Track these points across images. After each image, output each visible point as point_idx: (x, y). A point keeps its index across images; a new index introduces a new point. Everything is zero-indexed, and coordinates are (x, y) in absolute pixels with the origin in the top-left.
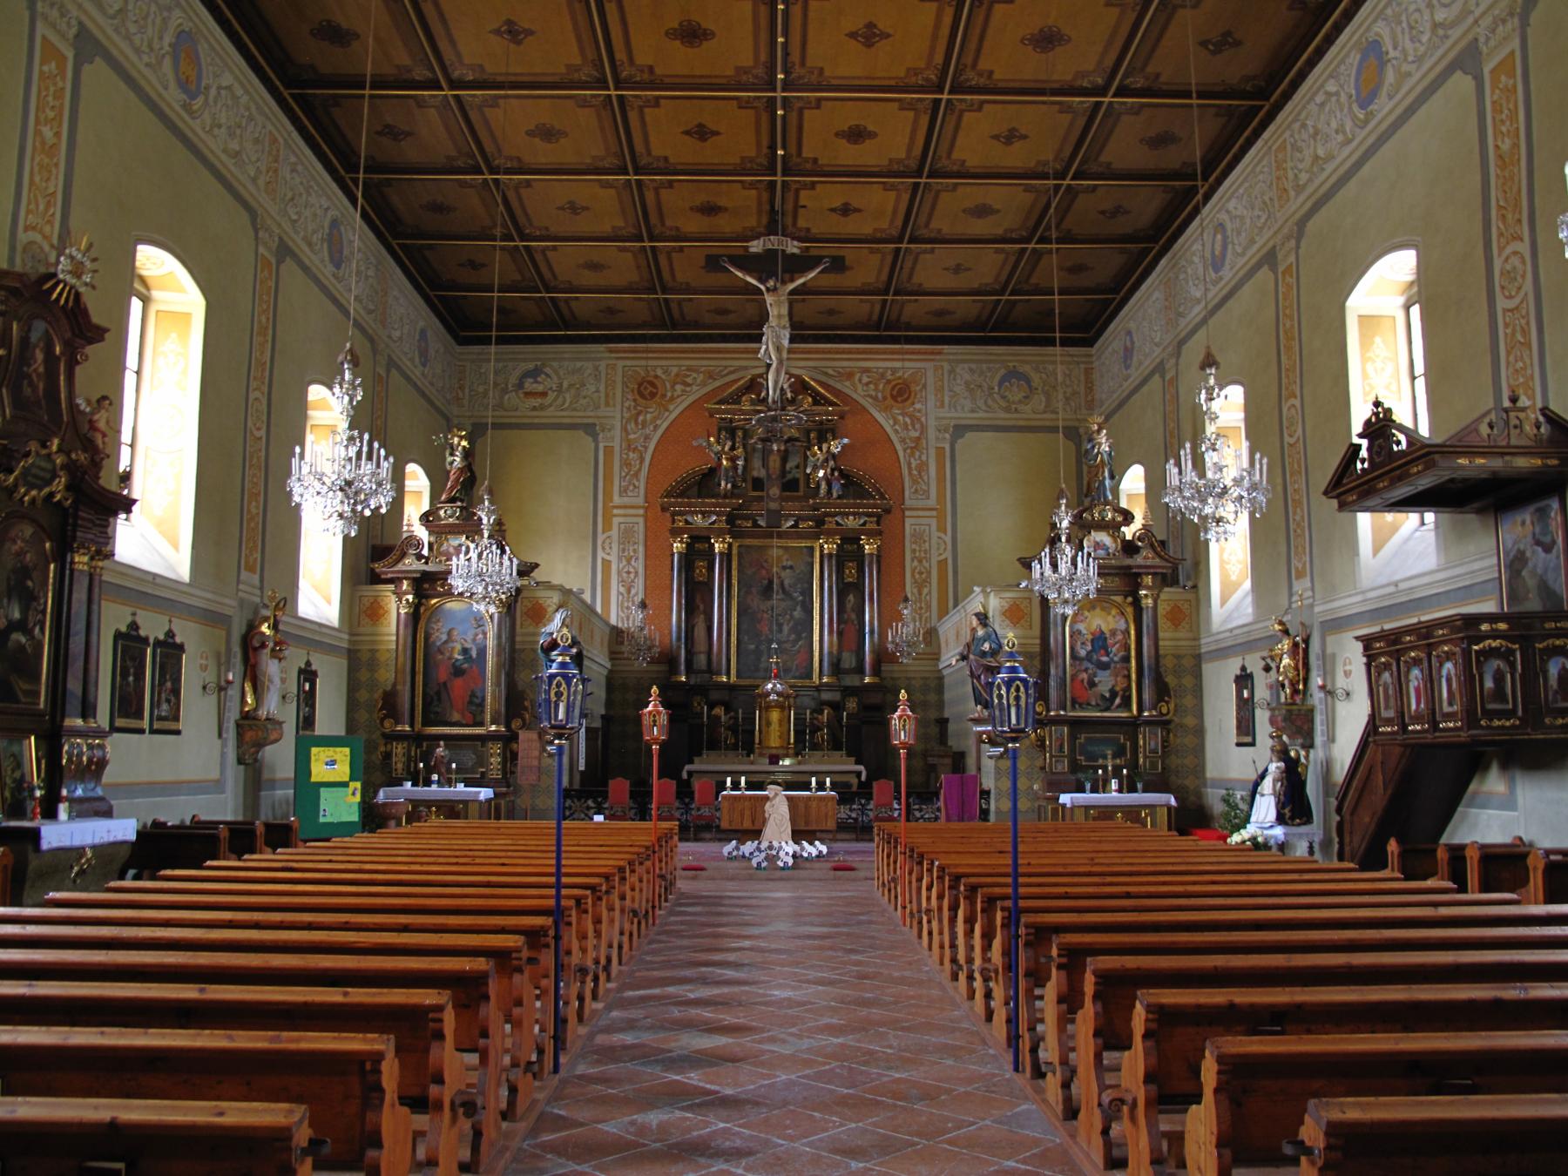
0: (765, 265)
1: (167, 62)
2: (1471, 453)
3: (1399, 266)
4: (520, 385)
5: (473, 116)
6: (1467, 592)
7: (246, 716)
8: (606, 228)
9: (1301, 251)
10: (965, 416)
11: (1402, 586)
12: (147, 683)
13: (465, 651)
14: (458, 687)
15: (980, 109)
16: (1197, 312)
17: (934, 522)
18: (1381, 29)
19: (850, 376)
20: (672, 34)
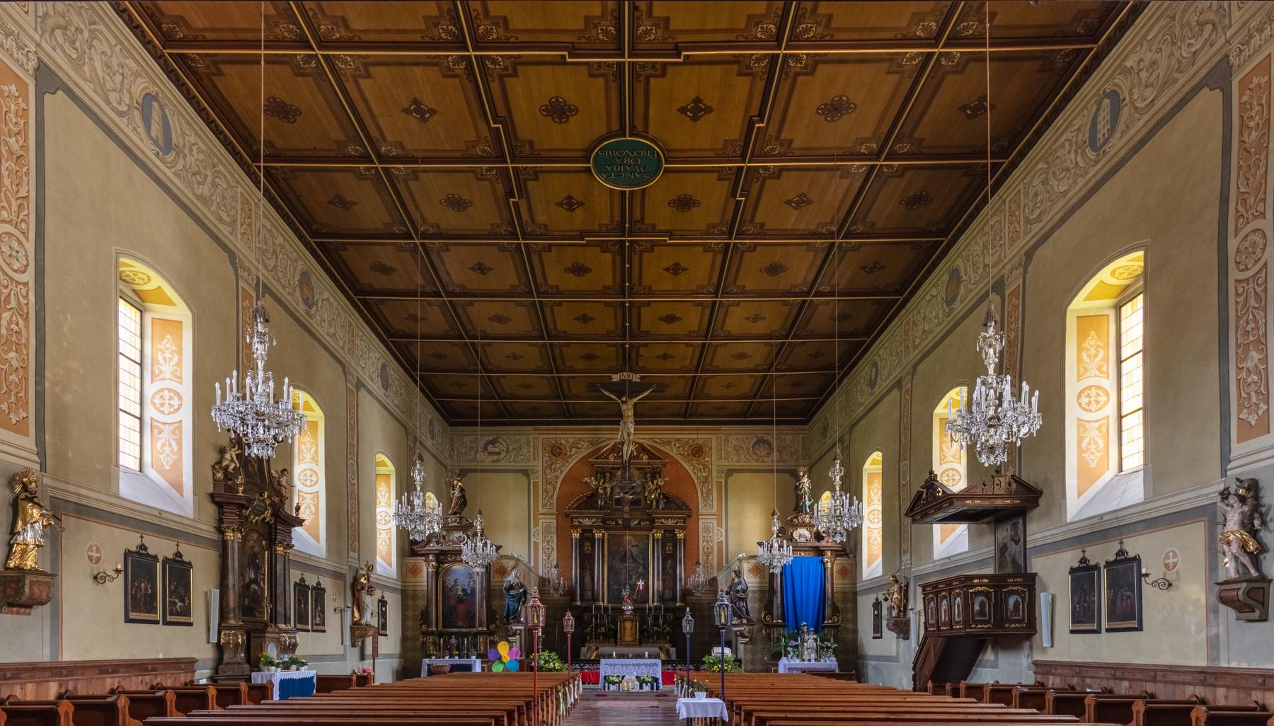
0: (624, 389)
1: (298, 290)
2: (973, 498)
3: (877, 456)
4: (485, 449)
5: (460, 310)
6: (982, 563)
7: (354, 623)
8: (532, 366)
9: (1030, 269)
10: (733, 463)
11: (1105, 518)
12: (309, 608)
13: (464, 590)
14: (461, 608)
15: (754, 250)
16: (861, 410)
17: (715, 522)
18: (959, 262)
19: (669, 443)
20: (569, 270)
